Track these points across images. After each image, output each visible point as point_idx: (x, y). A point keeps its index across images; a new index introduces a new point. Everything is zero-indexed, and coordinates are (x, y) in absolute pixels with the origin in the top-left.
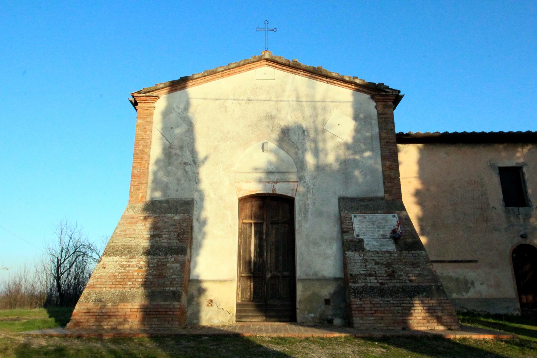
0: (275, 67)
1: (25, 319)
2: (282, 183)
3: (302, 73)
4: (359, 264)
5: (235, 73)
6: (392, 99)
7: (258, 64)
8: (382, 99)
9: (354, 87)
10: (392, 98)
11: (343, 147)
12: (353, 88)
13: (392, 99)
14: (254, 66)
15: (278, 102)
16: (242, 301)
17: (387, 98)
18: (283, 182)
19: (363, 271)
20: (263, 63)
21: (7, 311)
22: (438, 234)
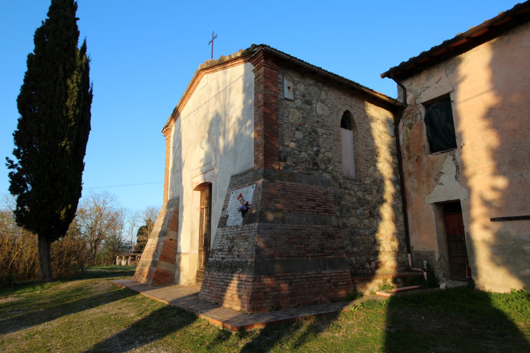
0: (202, 76)
1: (332, 310)
2: (208, 172)
3: (218, 68)
4: (219, 240)
5: (193, 91)
6: (262, 57)
7: (200, 77)
8: (256, 61)
9: (242, 61)
10: (260, 56)
11: (24, 230)
12: (242, 62)
13: (262, 57)
14: (199, 79)
15: (202, 106)
16: (199, 269)
17: (258, 58)
18: (209, 171)
19: (219, 246)
20: (202, 74)
21: (141, 264)
22: (522, 175)
